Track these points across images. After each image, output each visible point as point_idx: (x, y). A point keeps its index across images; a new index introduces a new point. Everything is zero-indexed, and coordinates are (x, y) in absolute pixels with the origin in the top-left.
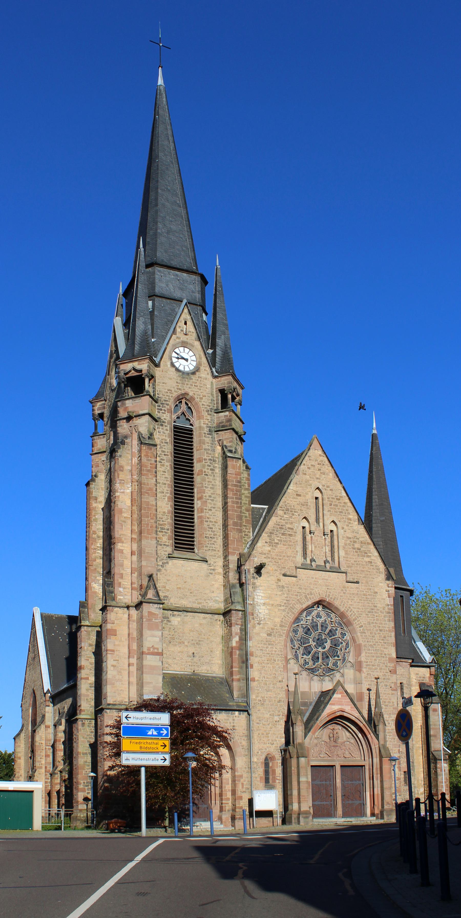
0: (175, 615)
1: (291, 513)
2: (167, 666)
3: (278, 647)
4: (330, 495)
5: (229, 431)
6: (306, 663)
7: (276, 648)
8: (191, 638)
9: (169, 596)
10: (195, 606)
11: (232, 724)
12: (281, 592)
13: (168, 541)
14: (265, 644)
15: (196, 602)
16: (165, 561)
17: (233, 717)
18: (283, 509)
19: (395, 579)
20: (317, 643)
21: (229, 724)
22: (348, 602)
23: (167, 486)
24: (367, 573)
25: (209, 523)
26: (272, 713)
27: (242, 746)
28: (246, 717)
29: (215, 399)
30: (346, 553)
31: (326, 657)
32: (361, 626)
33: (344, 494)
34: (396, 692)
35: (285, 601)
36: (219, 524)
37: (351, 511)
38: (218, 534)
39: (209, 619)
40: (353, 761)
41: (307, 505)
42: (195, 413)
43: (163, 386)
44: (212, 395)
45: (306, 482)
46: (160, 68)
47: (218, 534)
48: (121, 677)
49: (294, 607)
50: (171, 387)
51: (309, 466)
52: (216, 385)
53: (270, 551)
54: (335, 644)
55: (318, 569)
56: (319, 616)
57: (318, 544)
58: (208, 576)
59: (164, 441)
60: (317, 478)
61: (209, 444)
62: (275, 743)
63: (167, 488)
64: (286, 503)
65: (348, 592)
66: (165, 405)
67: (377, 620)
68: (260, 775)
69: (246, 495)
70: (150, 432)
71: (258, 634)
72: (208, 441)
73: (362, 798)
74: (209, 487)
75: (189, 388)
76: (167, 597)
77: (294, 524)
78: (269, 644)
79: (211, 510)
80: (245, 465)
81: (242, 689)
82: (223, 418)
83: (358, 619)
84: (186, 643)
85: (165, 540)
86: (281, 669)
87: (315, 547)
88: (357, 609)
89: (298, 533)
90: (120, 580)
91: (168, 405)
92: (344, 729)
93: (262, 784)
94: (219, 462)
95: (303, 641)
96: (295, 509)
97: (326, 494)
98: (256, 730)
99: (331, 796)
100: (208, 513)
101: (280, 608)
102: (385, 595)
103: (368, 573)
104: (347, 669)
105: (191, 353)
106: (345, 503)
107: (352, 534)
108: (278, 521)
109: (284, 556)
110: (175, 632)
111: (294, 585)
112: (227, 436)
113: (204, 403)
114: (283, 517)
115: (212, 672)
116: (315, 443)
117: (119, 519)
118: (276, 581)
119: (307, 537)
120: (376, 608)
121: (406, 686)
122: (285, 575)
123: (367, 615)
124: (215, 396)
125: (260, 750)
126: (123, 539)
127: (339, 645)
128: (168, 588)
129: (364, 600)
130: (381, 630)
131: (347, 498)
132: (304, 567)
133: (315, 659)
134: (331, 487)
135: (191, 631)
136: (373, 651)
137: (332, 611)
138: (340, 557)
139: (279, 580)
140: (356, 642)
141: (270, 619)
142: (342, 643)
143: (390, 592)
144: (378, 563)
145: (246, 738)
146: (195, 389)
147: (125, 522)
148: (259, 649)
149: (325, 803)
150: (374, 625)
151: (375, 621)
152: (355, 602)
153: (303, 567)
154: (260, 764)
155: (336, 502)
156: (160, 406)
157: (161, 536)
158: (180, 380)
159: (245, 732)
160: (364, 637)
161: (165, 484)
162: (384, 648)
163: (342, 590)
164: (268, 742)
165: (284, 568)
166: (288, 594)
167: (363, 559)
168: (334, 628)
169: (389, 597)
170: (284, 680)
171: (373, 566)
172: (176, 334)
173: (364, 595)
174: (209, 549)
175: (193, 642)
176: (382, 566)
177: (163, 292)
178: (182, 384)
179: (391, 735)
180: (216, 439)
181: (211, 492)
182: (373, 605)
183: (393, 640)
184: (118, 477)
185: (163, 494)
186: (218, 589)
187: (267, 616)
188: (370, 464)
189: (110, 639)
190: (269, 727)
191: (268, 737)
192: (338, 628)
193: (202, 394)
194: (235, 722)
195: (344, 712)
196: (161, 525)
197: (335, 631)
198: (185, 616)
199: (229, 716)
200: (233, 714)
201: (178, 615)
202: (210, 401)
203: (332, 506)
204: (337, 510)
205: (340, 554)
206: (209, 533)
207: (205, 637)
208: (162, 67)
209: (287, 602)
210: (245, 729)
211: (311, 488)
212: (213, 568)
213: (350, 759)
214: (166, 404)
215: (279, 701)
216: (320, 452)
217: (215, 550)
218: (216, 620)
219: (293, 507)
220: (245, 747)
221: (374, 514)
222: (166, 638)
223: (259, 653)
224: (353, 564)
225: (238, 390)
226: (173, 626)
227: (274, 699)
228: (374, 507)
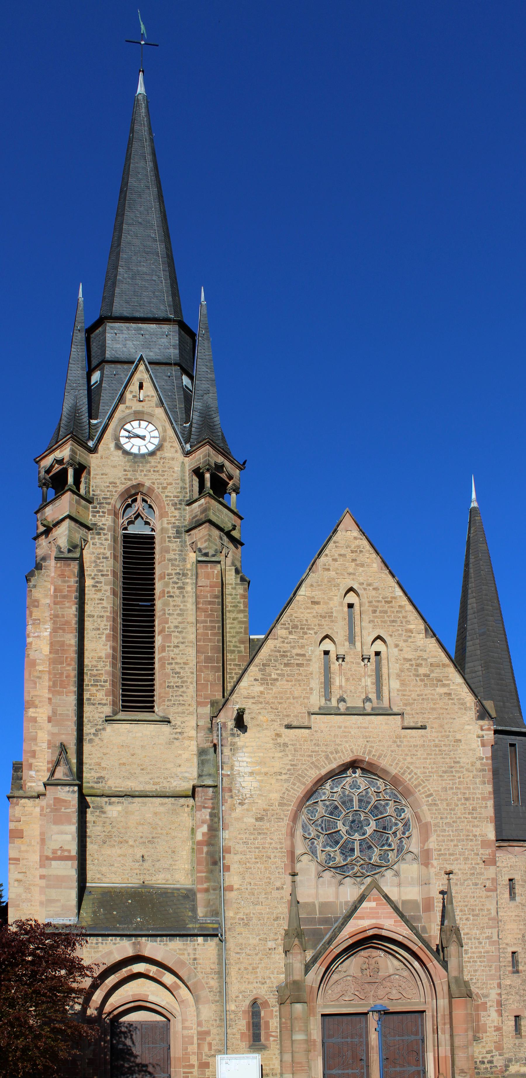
0: (114, 802)
1: (302, 631)
2: (99, 876)
3: (275, 838)
4: (373, 597)
5: (204, 526)
6: (330, 859)
7: (272, 839)
8: (140, 834)
9: (107, 776)
10: (150, 788)
11: (192, 956)
12: (283, 753)
13: (105, 698)
14: (251, 834)
15: (151, 782)
16: (101, 727)
18: (287, 626)
19: (494, 714)
20: (351, 827)
21: (186, 956)
22: (405, 759)
23: (105, 619)
24: (441, 711)
25: (173, 665)
26: (262, 936)
27: (209, 988)
28: (217, 945)
29: (188, 486)
30: (403, 683)
31: (367, 847)
32: (431, 795)
33: (399, 592)
34: (495, 893)
35: (289, 767)
36: (191, 665)
37: (412, 618)
38: (189, 680)
39: (170, 805)
40: (402, 1005)
43: (102, 478)
44: (183, 480)
45: (329, 582)
46: (141, 74)
47: (189, 680)
49: (306, 774)
50: (115, 479)
51: (334, 558)
52: (189, 466)
53: (262, 693)
55: (351, 712)
56: (355, 785)
57: (351, 675)
58: (170, 743)
59: (101, 556)
60: (350, 574)
61: (177, 552)
62: (268, 981)
63: (105, 623)
64: (293, 618)
65: (405, 743)
66: (105, 505)
67: (460, 783)
68: (240, 1029)
69: (240, 619)
70: (72, 542)
71: (238, 819)
72: (174, 548)
73: (423, 1062)
74: (175, 613)
75: (145, 475)
76: (103, 778)
77: (306, 647)
78: (260, 834)
80: (239, 576)
81: (211, 903)
82: (197, 510)
83: (424, 785)
84: (131, 842)
85: (101, 697)
86: (280, 870)
87: (347, 680)
88: (422, 769)
89: (314, 660)
90: (31, 761)
91: (109, 504)
92: (390, 956)
93: (244, 1043)
94: (192, 576)
96: (308, 625)
97: (365, 596)
98: (234, 964)
99: (361, 1060)
100: (173, 651)
101: (279, 777)
103: (444, 711)
104: (406, 863)
105: (151, 427)
106: (400, 606)
107: (415, 653)
108: (278, 645)
109: (288, 698)
110: (113, 827)
111: (305, 741)
112: (201, 534)
113: (169, 494)
114: (287, 638)
115: (174, 882)
117: (30, 674)
118: (274, 737)
119: (332, 666)
120: (458, 765)
121: (521, 883)
122: (289, 727)
123: (441, 776)
124: (187, 480)
126: (37, 702)
127: (391, 827)
128: (105, 766)
129: (435, 754)
130: (467, 799)
131: (405, 598)
132: (324, 712)
134: (375, 585)
135: (139, 824)
136: (452, 831)
137: (379, 777)
138: (391, 690)
139: (278, 735)
140: (421, 821)
141: (261, 795)
142: (396, 824)
143: (485, 738)
144: (463, 694)
145: (217, 976)
146: (154, 476)
147: (39, 678)
148: (241, 841)
149: (350, 1071)
150: (454, 791)
151: (457, 785)
153: (322, 712)
154: (240, 1014)
155: (383, 607)
156: (96, 508)
157: (95, 692)
158: (130, 467)
159: (215, 967)
161: (102, 617)
162: (473, 826)
163: (395, 742)
164: (255, 981)
165: (288, 716)
166: (294, 755)
167: (435, 690)
168: (383, 803)
169: (483, 745)
170: (285, 887)
171: (452, 699)
172: (124, 403)
173: (436, 746)
174: (174, 704)
175: (141, 840)
176: (469, 699)
177: (118, 356)
178: (133, 471)
179: (484, 961)
180: (188, 543)
181: (178, 620)
182: (452, 760)
183: (490, 811)
184: (31, 616)
185: (98, 632)
186: (187, 760)
187: (255, 791)
189: (14, 843)
190: (257, 957)
191: (256, 973)
192: (390, 802)
193: (167, 481)
194: (197, 952)
196: (95, 676)
197: (384, 806)
198: (130, 803)
199: (187, 944)
200: (194, 941)
201: (118, 803)
203: (378, 614)
204: (386, 618)
205: (391, 687)
206: (173, 681)
207: (162, 831)
208: (143, 71)
209: (292, 768)
210: (214, 963)
211: (339, 589)
212: (180, 731)
213: (400, 1001)
214: (106, 503)
215: (277, 919)
217: (183, 704)
218: (183, 806)
219: (305, 622)
221: (469, 628)
222: (99, 837)
223: (240, 847)
224: (415, 700)
225: (229, 469)
226: (110, 818)
227: (266, 916)
228: (469, 617)
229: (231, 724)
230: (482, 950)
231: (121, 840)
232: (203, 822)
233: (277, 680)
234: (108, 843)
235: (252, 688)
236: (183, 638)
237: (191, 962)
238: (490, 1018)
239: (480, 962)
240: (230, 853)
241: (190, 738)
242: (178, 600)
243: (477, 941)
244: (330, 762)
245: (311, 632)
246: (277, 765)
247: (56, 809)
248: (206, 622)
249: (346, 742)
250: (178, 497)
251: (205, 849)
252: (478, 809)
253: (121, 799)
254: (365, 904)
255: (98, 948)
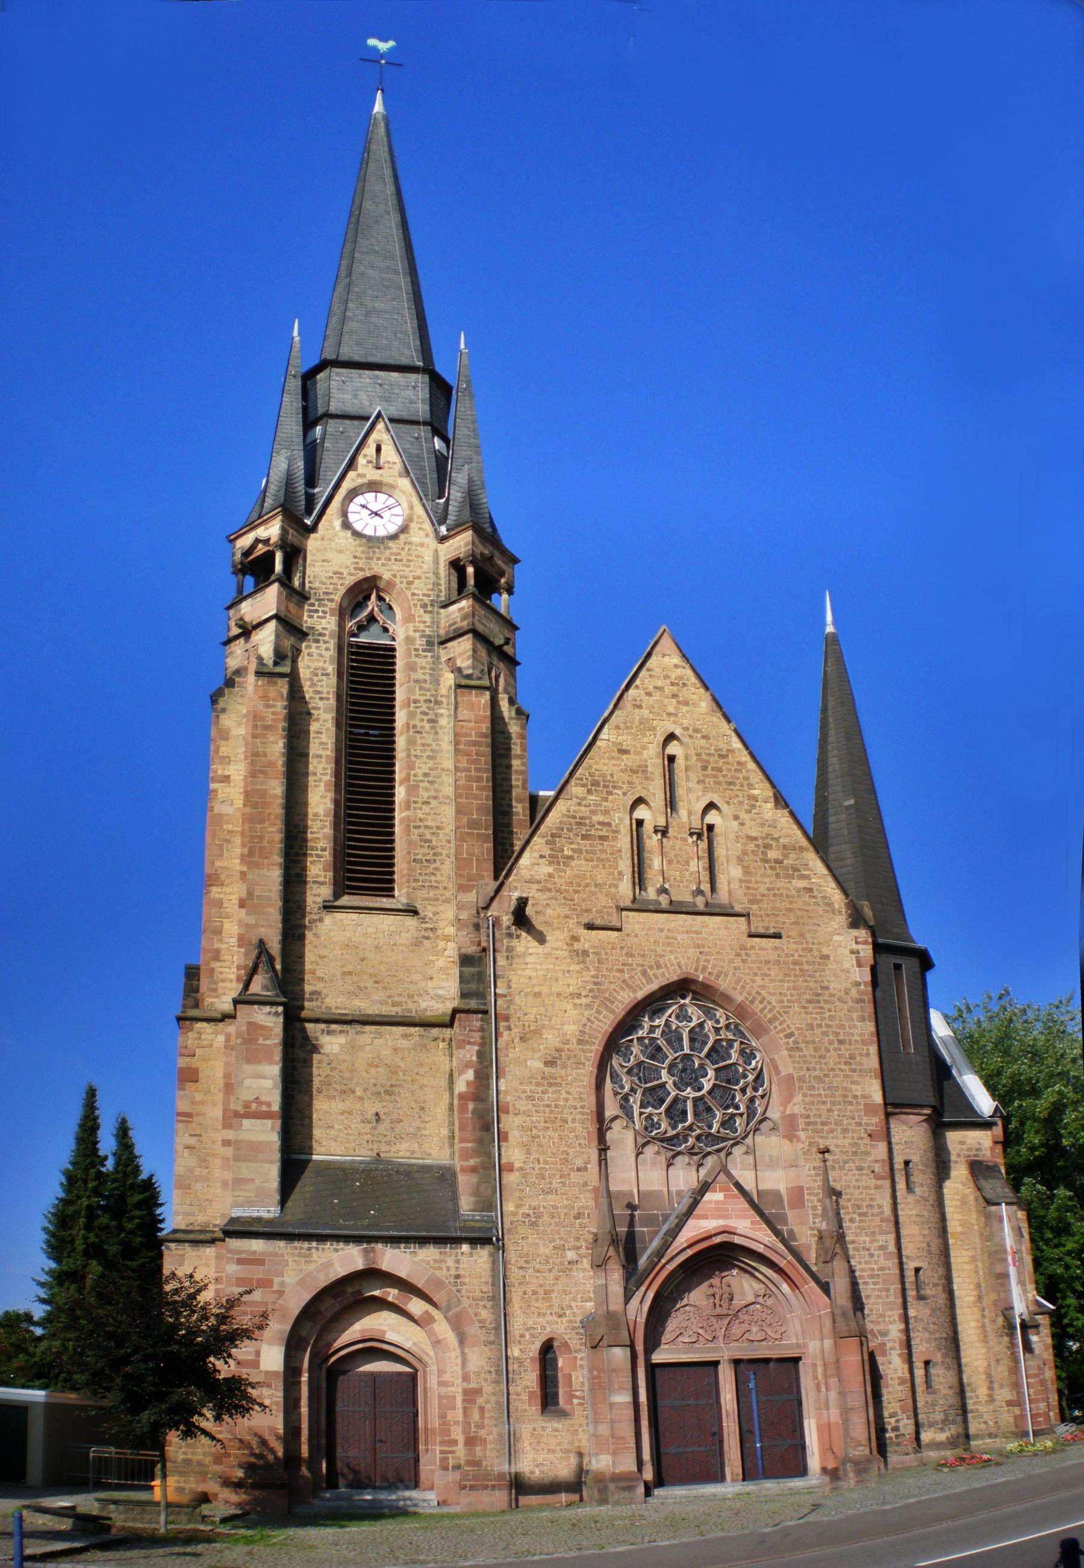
3: (574, 1091)
8: (373, 1081)
9: (324, 991)
11: (453, 1272)
12: (582, 966)
13: (323, 874)
14: (538, 1084)
15: (390, 1001)
16: (316, 917)
17: (456, 1255)
20: (681, 1078)
22: (754, 981)
23: (323, 760)
24: (799, 914)
25: (421, 830)
26: (558, 1242)
27: (480, 1321)
28: (491, 1255)
30: (747, 871)
32: (791, 1035)
33: (736, 744)
36: (447, 830)
38: (445, 852)
39: (417, 1038)
41: (645, 772)
42: (399, 615)
44: (437, 574)
47: (445, 852)
48: (206, 1171)
53: (550, 875)
54: (728, 1076)
55: (676, 909)
56: (683, 1016)
58: (417, 943)
59: (320, 672)
60: (669, 714)
63: (324, 765)
68: (527, 1387)
74: (425, 755)
75: (383, 565)
78: (550, 1085)
79: (429, 803)
83: (781, 1019)
84: (359, 1093)
85: (317, 872)
86: (582, 1141)
87: (670, 862)
88: (778, 997)
90: (215, 965)
91: (332, 601)
95: (723, 1092)
100: (421, 809)
101: (577, 1001)
102: (850, 962)
106: (739, 763)
109: (587, 885)
110: (332, 1069)
113: (416, 591)
114: (584, 799)
116: (666, 643)
120: (827, 992)
122: (590, 927)
123: (804, 1007)
125: (528, 1330)
126: (223, 877)
128: (322, 975)
130: (841, 1042)
131: (745, 752)
132: (639, 906)
133: (676, 1113)
139: (575, 938)
142: (745, 1076)
143: (862, 954)
146: (396, 567)
147: (228, 841)
148: (523, 1096)
151: (827, 1022)
152: (772, 981)
153: (636, 906)
154: (527, 1363)
155: (716, 762)
160: (798, 1059)
161: (320, 756)
163: (738, 955)
165: (588, 911)
166: (597, 969)
169: (859, 965)
171: (814, 897)
172: (356, 470)
175: (375, 1090)
176: (837, 897)
179: (878, 1283)
180: (443, 659)
188: (414, 258)
194: (461, 1266)
195: (734, 1234)
198: (357, 1033)
201: (341, 1032)
202: (431, 586)
203: (709, 772)
204: (721, 779)
214: (329, 600)
215: (578, 1216)
216: (676, 659)
219: (609, 778)
220: (487, 1324)
221: (831, 797)
223: (522, 1105)
224: (764, 895)
229: (507, 920)
230: (875, 1267)
231: (344, 1087)
232: (468, 1065)
233: (571, 858)
234: (324, 1093)
235: (536, 868)
236: (436, 791)
237: (452, 1280)
238: (892, 1366)
239: (874, 1283)
240: (508, 1113)
241: (447, 938)
242: (429, 739)
243: (866, 1253)
244: (649, 981)
245: (619, 792)
246: (573, 983)
247: (250, 1040)
248: (469, 770)
249: (671, 952)
250: (429, 596)
251: (471, 1106)
252: (858, 1058)
253: (345, 1027)
254: (708, 1196)
255: (310, 1256)
